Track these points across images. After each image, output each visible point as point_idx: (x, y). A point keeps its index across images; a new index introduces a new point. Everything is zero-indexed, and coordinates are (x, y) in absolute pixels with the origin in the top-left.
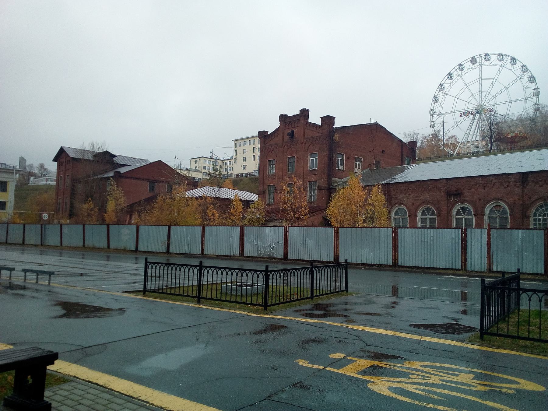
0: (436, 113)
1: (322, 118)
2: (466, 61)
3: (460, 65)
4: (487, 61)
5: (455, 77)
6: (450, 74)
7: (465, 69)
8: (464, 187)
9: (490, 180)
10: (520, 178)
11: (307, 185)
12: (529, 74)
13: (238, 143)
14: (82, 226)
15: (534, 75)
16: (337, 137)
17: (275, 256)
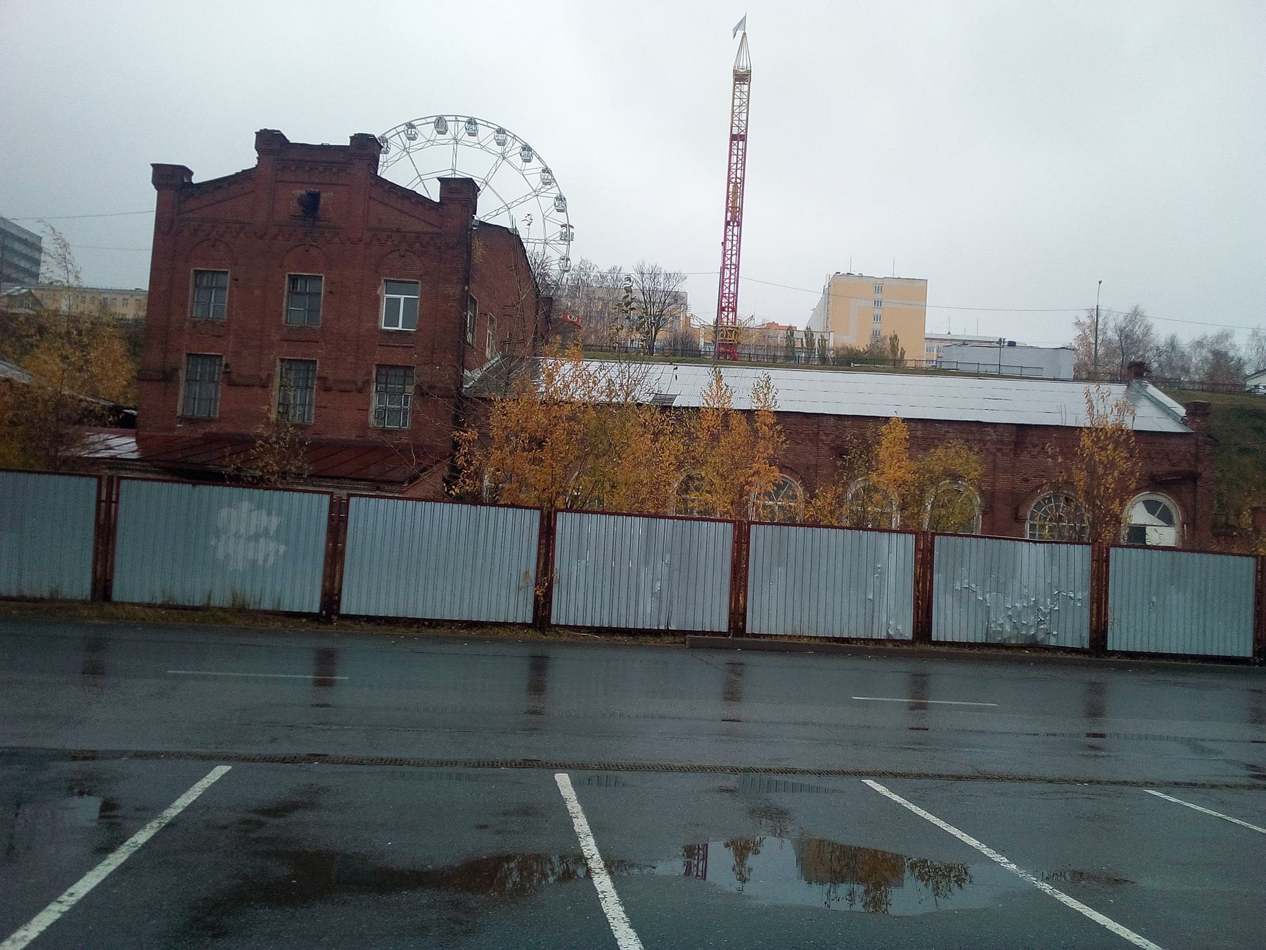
3: (410, 126)
7: (420, 139)
9: (942, 432)
10: (1011, 435)
11: (370, 373)
12: (555, 191)
15: (564, 195)
17: (1053, 642)
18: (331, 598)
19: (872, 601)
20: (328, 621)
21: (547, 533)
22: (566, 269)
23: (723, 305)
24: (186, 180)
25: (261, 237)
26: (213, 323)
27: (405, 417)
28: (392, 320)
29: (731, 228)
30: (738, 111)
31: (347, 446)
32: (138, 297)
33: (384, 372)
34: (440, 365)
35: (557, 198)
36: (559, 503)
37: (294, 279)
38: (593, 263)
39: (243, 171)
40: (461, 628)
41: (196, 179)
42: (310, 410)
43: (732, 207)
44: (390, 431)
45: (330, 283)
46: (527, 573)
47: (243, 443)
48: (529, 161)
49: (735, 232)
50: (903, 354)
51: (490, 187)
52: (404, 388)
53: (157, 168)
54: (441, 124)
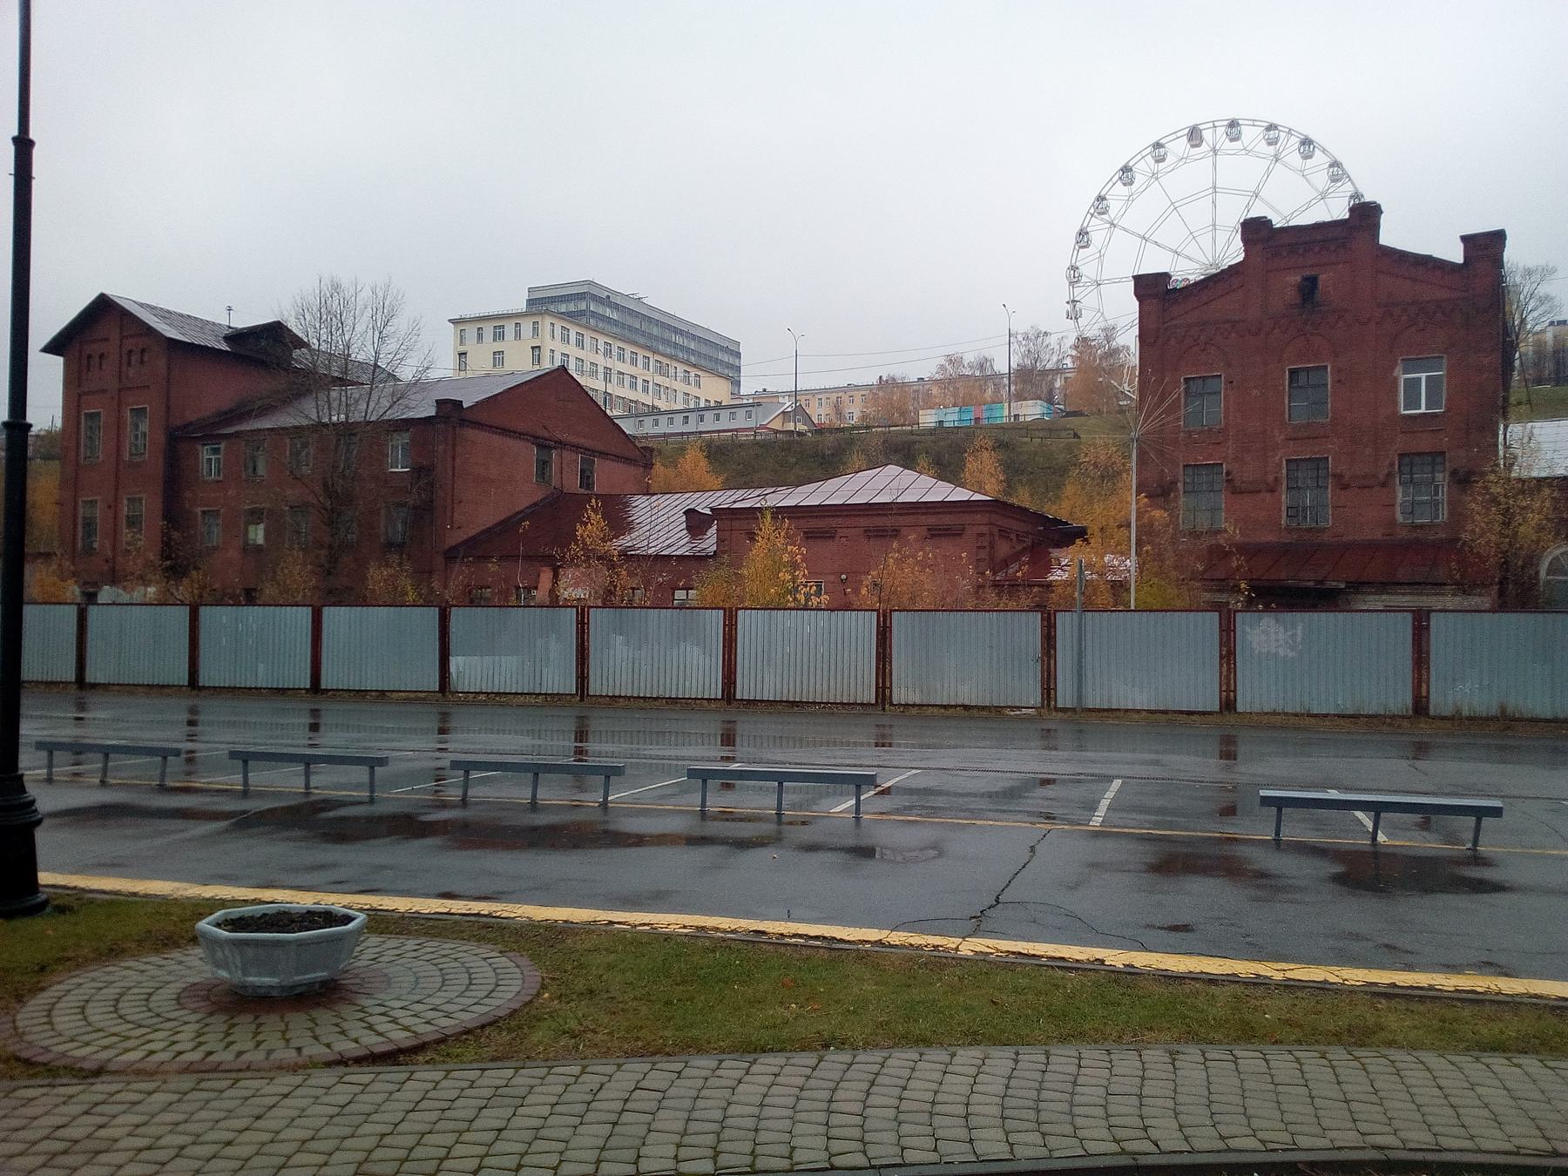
0: (1084, 279)
1: (1464, 239)
3: (1158, 145)
4: (1232, 140)
5: (1139, 179)
6: (1126, 169)
7: (1170, 159)
11: (1392, 465)
13: (471, 331)
21: (582, 678)
28: (1413, 401)
31: (1372, 547)
34: (1478, 445)
37: (1292, 372)
44: (1422, 526)
51: (1262, 200)
52: (1433, 478)
53: (1139, 280)
54: (1194, 135)
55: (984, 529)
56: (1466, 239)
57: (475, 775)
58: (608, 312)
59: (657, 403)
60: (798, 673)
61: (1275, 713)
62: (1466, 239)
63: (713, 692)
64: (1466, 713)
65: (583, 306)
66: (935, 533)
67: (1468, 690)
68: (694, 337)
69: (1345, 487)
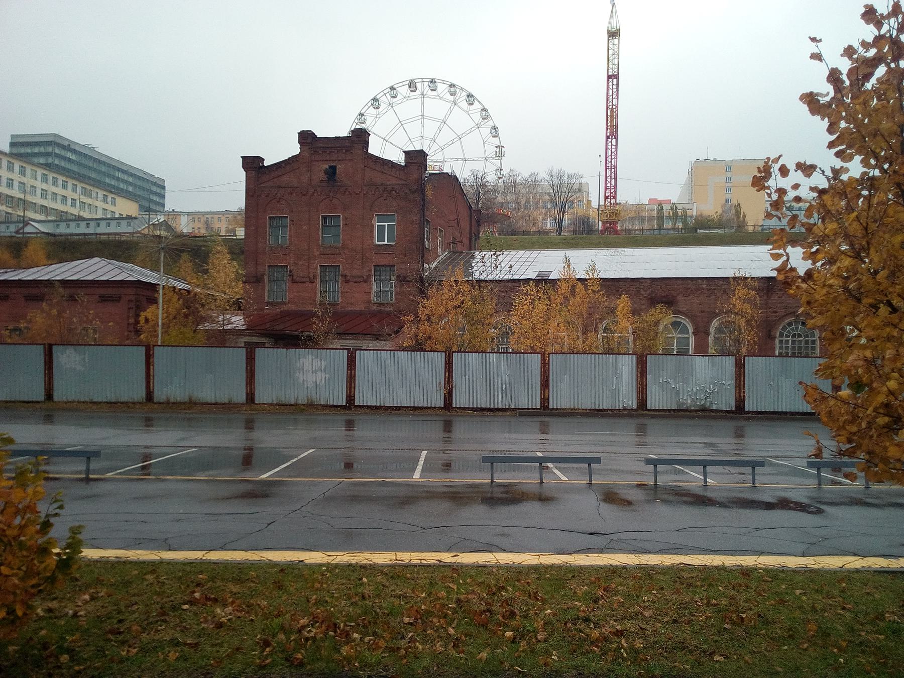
2: (401, 84)
3: (393, 88)
4: (432, 90)
6: (375, 100)
7: (399, 97)
8: (678, 292)
11: (370, 271)
12: (491, 123)
14: (144, 353)
15: (497, 125)
16: (429, 191)
17: (715, 407)
18: (351, 398)
19: (615, 390)
20: (350, 408)
22: (501, 176)
23: (607, 195)
24: (261, 165)
25: (305, 195)
26: (282, 247)
27: (392, 295)
28: (381, 238)
29: (610, 140)
30: (612, 58)
31: (360, 314)
32: (227, 216)
33: (378, 269)
34: (410, 263)
35: (492, 128)
36: (455, 349)
37: (324, 218)
38: (518, 172)
39: (293, 156)
40: (410, 410)
41: (267, 163)
42: (338, 293)
43: (610, 126)
44: (383, 304)
45: (345, 219)
46: (440, 383)
47: (306, 316)
48: (472, 104)
49: (614, 143)
50: (744, 216)
53: (244, 158)
54: (412, 85)
55: (132, 297)
56: (407, 153)
57: (660, 468)
58: (69, 155)
59: (83, 214)
60: (471, 392)
61: (73, 402)
62: (407, 153)
63: (340, 400)
64: (172, 400)
65: (50, 149)
66: (104, 299)
67: (173, 389)
68: (131, 175)
69: (347, 282)
